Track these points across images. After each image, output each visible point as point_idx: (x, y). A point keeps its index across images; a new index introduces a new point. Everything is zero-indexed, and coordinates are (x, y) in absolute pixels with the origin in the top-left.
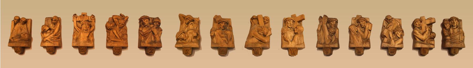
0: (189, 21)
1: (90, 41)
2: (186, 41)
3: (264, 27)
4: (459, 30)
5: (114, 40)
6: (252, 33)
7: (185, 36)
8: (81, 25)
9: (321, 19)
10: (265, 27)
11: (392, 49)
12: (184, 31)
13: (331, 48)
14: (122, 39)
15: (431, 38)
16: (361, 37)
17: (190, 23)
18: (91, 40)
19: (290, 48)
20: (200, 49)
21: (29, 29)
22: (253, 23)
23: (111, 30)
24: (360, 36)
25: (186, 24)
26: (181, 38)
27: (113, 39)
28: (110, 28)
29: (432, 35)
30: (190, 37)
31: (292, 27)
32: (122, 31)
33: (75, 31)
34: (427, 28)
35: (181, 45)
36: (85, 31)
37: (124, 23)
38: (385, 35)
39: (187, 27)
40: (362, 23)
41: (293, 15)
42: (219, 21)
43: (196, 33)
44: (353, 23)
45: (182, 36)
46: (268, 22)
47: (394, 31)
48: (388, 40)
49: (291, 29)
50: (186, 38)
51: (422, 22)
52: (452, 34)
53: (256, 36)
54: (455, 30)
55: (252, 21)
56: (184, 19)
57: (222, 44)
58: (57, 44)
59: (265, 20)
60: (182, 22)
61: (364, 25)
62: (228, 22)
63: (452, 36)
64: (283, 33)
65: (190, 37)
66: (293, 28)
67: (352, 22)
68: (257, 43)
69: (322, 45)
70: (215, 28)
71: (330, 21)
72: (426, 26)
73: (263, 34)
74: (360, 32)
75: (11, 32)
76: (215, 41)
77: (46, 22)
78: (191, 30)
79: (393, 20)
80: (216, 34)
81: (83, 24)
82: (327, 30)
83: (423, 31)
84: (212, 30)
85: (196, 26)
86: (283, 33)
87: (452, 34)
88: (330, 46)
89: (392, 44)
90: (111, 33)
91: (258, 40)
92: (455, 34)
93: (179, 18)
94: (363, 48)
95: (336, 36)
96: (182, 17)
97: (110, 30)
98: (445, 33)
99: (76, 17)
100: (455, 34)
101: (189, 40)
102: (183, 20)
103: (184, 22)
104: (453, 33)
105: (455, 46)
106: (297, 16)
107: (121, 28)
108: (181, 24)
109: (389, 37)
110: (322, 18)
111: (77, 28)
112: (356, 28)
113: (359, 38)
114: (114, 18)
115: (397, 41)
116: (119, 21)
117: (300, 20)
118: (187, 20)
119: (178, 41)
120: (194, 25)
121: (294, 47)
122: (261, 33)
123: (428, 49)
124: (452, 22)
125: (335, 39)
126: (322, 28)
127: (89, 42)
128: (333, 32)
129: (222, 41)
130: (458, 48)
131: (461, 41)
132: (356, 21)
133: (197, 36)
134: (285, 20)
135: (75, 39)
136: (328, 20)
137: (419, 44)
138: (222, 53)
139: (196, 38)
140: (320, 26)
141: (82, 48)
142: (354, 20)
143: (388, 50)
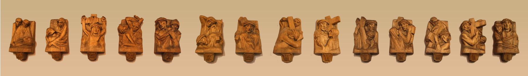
0: (211, 24)
1: (101, 45)
2: (207, 45)
3: (295, 30)
4: (512, 33)
5: (127, 45)
6: (282, 37)
7: (207, 40)
8: (90, 28)
9: (359, 21)
10: (295, 30)
11: (437, 55)
12: (206, 35)
13: (369, 54)
14: (136, 44)
15: (481, 43)
16: (403, 41)
17: (212, 25)
18: (102, 45)
19: (323, 53)
20: (223, 54)
21: (32, 33)
22: (283, 26)
23: (124, 34)
24: (402, 41)
25: (207, 27)
26: (202, 43)
27: (126, 44)
28: (123, 31)
29: (482, 39)
30: (212, 42)
31: (325, 31)
32: (136, 35)
33: (83, 35)
34: (476, 32)
35: (202, 50)
36: (95, 34)
37: (139, 25)
38: (429, 39)
39: (209, 30)
40: (405, 26)
41: (327, 17)
42: (245, 23)
43: (219, 36)
44: (395, 25)
45: (204, 40)
46: (299, 25)
47: (440, 35)
48: (433, 44)
49: (325, 32)
50: (208, 43)
51: (471, 25)
52: (505, 38)
53: (286, 40)
54: (508, 34)
55: (282, 23)
56: (206, 22)
57: (248, 50)
58: (63, 49)
59: (296, 23)
60: (203, 25)
61: (407, 28)
62: (254, 25)
63: (505, 40)
64: (316, 36)
65: (212, 42)
66: (327, 32)
67: (393, 25)
68: (287, 48)
69: (360, 50)
70: (240, 31)
71: (368, 23)
72: (476, 30)
73: (294, 38)
74: (401, 35)
75: (13, 35)
76: (239, 46)
77: (52, 25)
78: (213, 34)
79: (439, 22)
80: (241, 38)
81: (93, 27)
82: (365, 33)
83: (473, 34)
84: (237, 34)
85: (219, 29)
86: (316, 36)
87: (505, 38)
88: (368, 52)
89: (438, 50)
90: (123, 37)
91: (288, 45)
92: (508, 38)
93: (200, 20)
94: (405, 54)
95: (375, 40)
96: (203, 19)
97: (122, 33)
98: (497, 37)
99: (85, 19)
100: (508, 38)
101: (211, 45)
102: (204, 22)
103: (206, 25)
104: (506, 36)
105: (508, 51)
106: (331, 18)
107: (135, 32)
108: (202, 27)
109: (434, 41)
110: (360, 20)
111: (86, 31)
112: (397, 31)
113: (401, 43)
114: (128, 20)
115: (443, 46)
116: (133, 23)
117: (335, 23)
118: (208, 22)
119: (199, 46)
120: (217, 28)
121: (329, 52)
122: (292, 36)
123: (478, 55)
124: (505, 24)
125: (374, 43)
126: (359, 31)
127: (100, 47)
128: (372, 35)
129: (248, 46)
130: (511, 54)
131: (514, 46)
132: (398, 23)
133: (220, 40)
134: (318, 22)
135: (84, 43)
136: (366, 23)
137: (468, 49)
138: (248, 60)
139: (219, 43)
140: (358, 29)
141: (92, 53)
142: (395, 22)
143: (433, 56)
